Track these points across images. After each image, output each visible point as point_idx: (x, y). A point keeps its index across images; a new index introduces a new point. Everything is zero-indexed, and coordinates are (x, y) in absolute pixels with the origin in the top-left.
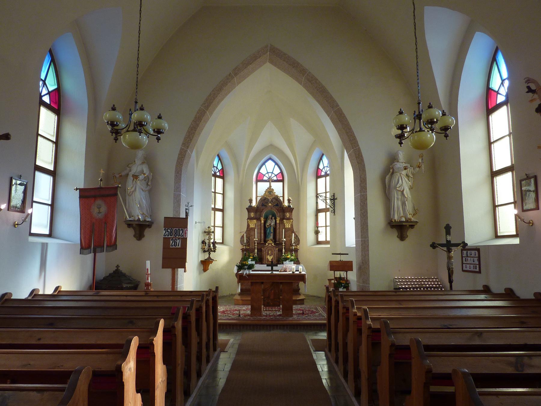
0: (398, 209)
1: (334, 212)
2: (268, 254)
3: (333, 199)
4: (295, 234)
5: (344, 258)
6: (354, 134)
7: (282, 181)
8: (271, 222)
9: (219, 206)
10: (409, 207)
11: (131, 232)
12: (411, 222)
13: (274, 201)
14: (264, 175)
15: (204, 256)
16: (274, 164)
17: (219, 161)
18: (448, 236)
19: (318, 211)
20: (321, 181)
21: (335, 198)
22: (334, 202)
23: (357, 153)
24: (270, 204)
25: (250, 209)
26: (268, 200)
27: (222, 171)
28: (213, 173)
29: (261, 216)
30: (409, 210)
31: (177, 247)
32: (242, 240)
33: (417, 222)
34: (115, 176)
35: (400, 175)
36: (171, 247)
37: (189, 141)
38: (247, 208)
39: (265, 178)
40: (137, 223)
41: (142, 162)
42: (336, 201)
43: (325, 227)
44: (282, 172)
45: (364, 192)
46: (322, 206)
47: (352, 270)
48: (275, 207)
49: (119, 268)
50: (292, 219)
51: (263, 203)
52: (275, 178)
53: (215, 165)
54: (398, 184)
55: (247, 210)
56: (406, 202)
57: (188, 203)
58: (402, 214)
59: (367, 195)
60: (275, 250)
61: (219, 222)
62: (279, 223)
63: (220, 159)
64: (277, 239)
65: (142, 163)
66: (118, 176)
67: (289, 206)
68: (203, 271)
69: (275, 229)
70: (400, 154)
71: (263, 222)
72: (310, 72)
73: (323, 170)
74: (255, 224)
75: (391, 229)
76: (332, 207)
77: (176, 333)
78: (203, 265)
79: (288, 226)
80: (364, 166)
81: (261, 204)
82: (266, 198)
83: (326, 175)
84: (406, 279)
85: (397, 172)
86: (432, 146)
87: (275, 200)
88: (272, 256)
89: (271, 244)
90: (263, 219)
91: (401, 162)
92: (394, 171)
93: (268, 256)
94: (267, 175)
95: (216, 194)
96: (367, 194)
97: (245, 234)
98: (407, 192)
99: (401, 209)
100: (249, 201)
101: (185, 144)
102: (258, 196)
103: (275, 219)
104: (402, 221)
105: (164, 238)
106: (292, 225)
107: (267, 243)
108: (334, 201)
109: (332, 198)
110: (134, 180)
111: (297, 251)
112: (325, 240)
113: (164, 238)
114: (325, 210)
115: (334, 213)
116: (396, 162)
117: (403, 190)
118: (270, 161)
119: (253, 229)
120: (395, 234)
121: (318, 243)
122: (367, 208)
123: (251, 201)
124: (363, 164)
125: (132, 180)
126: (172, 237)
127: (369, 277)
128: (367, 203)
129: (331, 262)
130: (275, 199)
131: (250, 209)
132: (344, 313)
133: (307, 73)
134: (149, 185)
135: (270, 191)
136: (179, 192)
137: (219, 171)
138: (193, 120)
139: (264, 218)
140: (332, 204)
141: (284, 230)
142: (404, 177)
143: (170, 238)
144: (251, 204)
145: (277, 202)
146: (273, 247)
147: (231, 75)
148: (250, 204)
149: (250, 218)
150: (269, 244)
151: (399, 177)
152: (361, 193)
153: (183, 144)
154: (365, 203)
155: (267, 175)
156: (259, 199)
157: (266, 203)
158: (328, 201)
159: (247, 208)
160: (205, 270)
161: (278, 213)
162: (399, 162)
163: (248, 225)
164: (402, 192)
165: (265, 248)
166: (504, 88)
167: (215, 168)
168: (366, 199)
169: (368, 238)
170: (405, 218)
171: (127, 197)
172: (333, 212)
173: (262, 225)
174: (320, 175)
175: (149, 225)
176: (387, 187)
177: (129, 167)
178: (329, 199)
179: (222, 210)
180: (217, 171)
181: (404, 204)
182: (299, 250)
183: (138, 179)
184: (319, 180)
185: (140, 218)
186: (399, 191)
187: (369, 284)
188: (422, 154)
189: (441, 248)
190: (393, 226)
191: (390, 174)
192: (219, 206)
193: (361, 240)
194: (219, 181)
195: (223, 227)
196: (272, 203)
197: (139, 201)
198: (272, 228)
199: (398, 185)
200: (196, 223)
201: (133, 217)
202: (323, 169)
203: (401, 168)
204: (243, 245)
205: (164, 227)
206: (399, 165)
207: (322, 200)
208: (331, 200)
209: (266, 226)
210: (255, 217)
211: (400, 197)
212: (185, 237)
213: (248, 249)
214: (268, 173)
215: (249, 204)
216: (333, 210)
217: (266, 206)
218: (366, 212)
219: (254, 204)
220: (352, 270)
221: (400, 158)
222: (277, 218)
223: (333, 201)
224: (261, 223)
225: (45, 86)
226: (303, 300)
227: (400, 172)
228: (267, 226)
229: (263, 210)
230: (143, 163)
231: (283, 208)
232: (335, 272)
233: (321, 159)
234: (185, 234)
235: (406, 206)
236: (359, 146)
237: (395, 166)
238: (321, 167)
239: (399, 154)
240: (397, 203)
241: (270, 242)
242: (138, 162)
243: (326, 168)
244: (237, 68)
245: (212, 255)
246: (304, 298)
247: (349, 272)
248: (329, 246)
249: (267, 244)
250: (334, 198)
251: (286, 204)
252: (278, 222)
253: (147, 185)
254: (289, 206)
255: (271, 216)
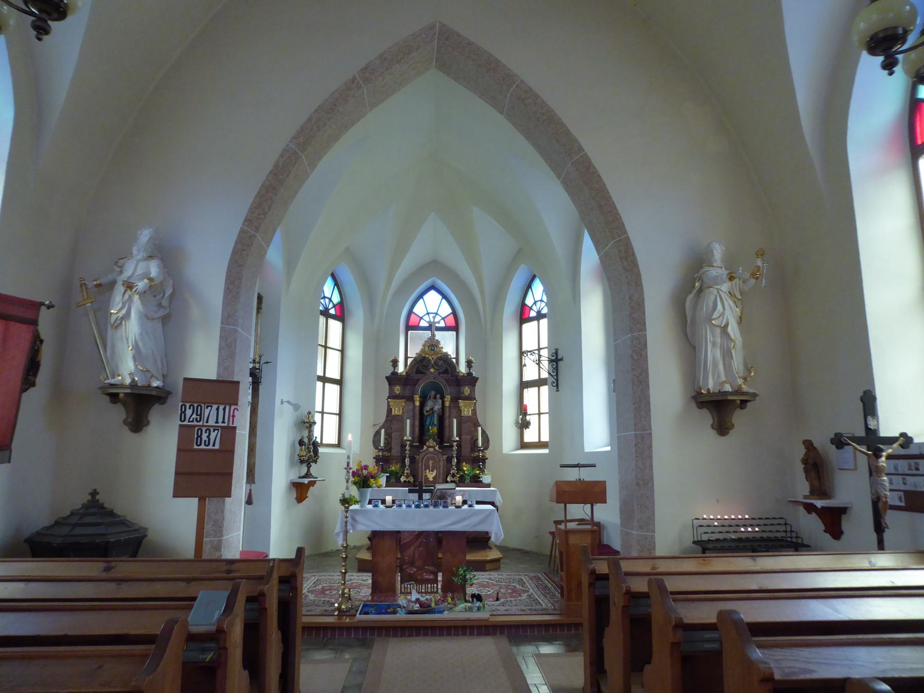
0: (715, 365)
1: (557, 385)
2: (427, 467)
3: (555, 360)
4: (482, 428)
5: (587, 475)
6: (615, 208)
7: (455, 328)
8: (434, 405)
9: (333, 372)
10: (737, 363)
11: (118, 414)
12: (746, 394)
13: (440, 364)
14: (421, 318)
15: (300, 471)
16: (440, 297)
17: (334, 288)
18: (869, 418)
19: (524, 385)
20: (529, 329)
21: (559, 358)
22: (557, 366)
23: (623, 250)
24: (432, 370)
25: (393, 379)
26: (429, 361)
27: (341, 306)
28: (321, 308)
29: (413, 393)
30: (738, 368)
31: (210, 447)
32: (376, 439)
33: (755, 395)
34: (85, 284)
35: (718, 292)
36: (195, 447)
37: (259, 215)
38: (387, 378)
39: (423, 324)
40: (128, 391)
41: (149, 255)
42: (560, 363)
43: (537, 416)
44: (454, 313)
45: (640, 331)
46: (531, 373)
47: (604, 501)
48: (441, 375)
49: (97, 497)
50: (475, 399)
51: (418, 368)
52: (442, 324)
53: (327, 294)
55: (388, 381)
56: (733, 351)
57: (260, 357)
58: (723, 378)
60: (442, 459)
61: (332, 405)
62: (450, 407)
63: (336, 284)
64: (446, 439)
65: (643, 687)
66: (91, 284)
67: (470, 374)
68: (295, 501)
69: (441, 419)
71: (417, 404)
72: (522, 81)
73: (534, 308)
74: (403, 409)
75: (699, 410)
76: (552, 376)
77: (267, 607)
78: (297, 490)
79: (467, 412)
80: (638, 275)
81: (415, 370)
82: (425, 357)
83: (540, 316)
84: (713, 519)
85: (711, 287)
87: (442, 362)
88: (435, 470)
89: (434, 447)
90: (418, 399)
91: (717, 267)
92: (705, 286)
93: (428, 471)
94: (426, 318)
95: (328, 350)
97: (383, 431)
98: (733, 330)
99: (721, 367)
100: (391, 364)
101: (250, 220)
102: (409, 356)
103: (442, 398)
104: (726, 392)
105: (180, 426)
106: (474, 411)
107: (425, 445)
108: (557, 364)
109: (554, 358)
110: (127, 292)
111: (485, 461)
112: (537, 440)
113: (180, 426)
114: (539, 383)
115: (557, 388)
116: (706, 266)
117: (727, 325)
118: (433, 293)
119: (400, 419)
120: (706, 418)
121: (524, 445)
122: (647, 364)
123: (395, 363)
125: (123, 292)
126: (201, 423)
127: (654, 515)
129: (558, 484)
130: (443, 360)
131: (393, 379)
132: (382, 469)
133: (517, 83)
134: (163, 307)
135: (433, 345)
136: (234, 325)
137: (334, 306)
138: (271, 172)
139: (420, 397)
140: (554, 369)
141: (455, 421)
142: (727, 297)
143: (194, 426)
144: (395, 369)
145: (446, 365)
146: (437, 452)
147: (356, 81)
148: (393, 370)
149: (392, 396)
150: (429, 447)
151: (716, 296)
152: (633, 333)
153: (246, 220)
154: (641, 355)
155: (426, 318)
156: (410, 361)
157: (424, 368)
158: (545, 364)
159: (387, 378)
160: (300, 498)
161: (448, 387)
162: (713, 266)
163: (389, 411)
164: (724, 329)
165: (421, 456)
167: (327, 300)
168: (646, 345)
169: (651, 430)
170: (731, 386)
171: (110, 332)
172: (554, 385)
173: (417, 410)
174: (526, 316)
175: (159, 397)
176: (689, 320)
177: (118, 266)
178: (547, 359)
179: (340, 382)
180: (331, 305)
181: (727, 354)
182: (487, 459)
183: (134, 290)
184: (525, 326)
185: (136, 379)
186: (718, 326)
187: (654, 532)
189: (858, 447)
190: (702, 402)
191: (695, 291)
192: (333, 372)
193: (636, 435)
194: (335, 327)
195: (340, 415)
196: (437, 368)
197: (136, 341)
198: (436, 415)
200: (282, 403)
201: (120, 378)
202: (532, 305)
203: (722, 278)
204: (378, 449)
205: (182, 402)
206: (717, 271)
207: (535, 360)
208: (550, 361)
209: (425, 412)
210: (402, 394)
211: (718, 340)
212: (231, 425)
213: (388, 456)
214: (428, 314)
215: (392, 369)
216: (555, 382)
217: (424, 373)
218: (135, 598)
219: (401, 369)
220: (604, 501)
221: (716, 258)
222: (445, 397)
223: (555, 363)
224: (414, 406)
225: (331, 302)
226: (497, 561)
227: (718, 287)
228: (427, 412)
229: (418, 380)
230: (150, 257)
231: (457, 376)
232: (567, 505)
233: (529, 286)
234: (231, 418)
235: (732, 359)
236: (627, 234)
237: (708, 272)
238: (529, 301)
240: (712, 353)
241: (431, 443)
242: (138, 252)
243: (534, 306)
244: (370, 68)
245: (314, 469)
246: (501, 556)
247: (597, 507)
248: (546, 451)
249: (425, 447)
250: (557, 357)
251: (463, 368)
252: (447, 404)
253: (160, 305)
254: (470, 374)
255: (433, 393)
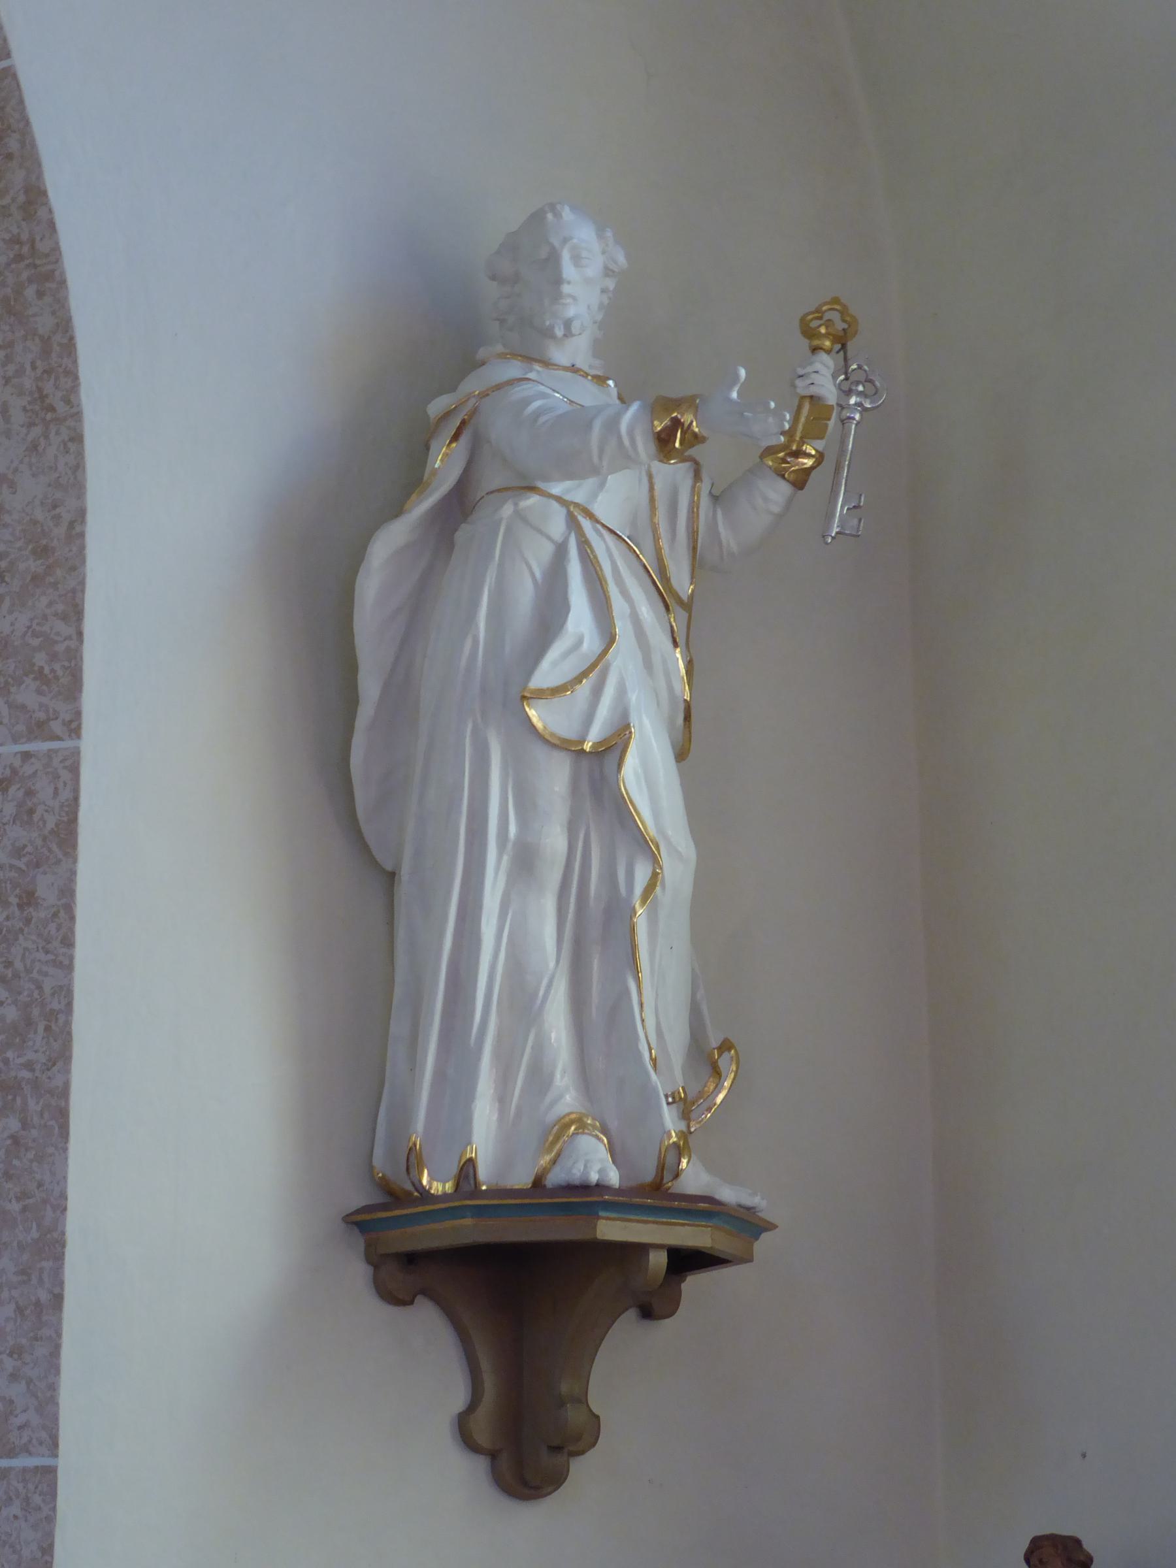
35: (573, 523)
45: (39, 730)
54: (554, 652)
59: (75, 770)
70: (577, 259)
86: (677, 431)
92: (492, 477)
96: (76, 753)
124: (45, 323)
128: (68, 892)
151: (561, 552)
154: (29, 899)
166: (823, 375)
169: (53, 1446)
176: (370, 687)
188: (836, 300)
190: (411, 1260)
191: (422, 506)
199: (545, 664)
235: (636, 971)
239: (566, 256)
